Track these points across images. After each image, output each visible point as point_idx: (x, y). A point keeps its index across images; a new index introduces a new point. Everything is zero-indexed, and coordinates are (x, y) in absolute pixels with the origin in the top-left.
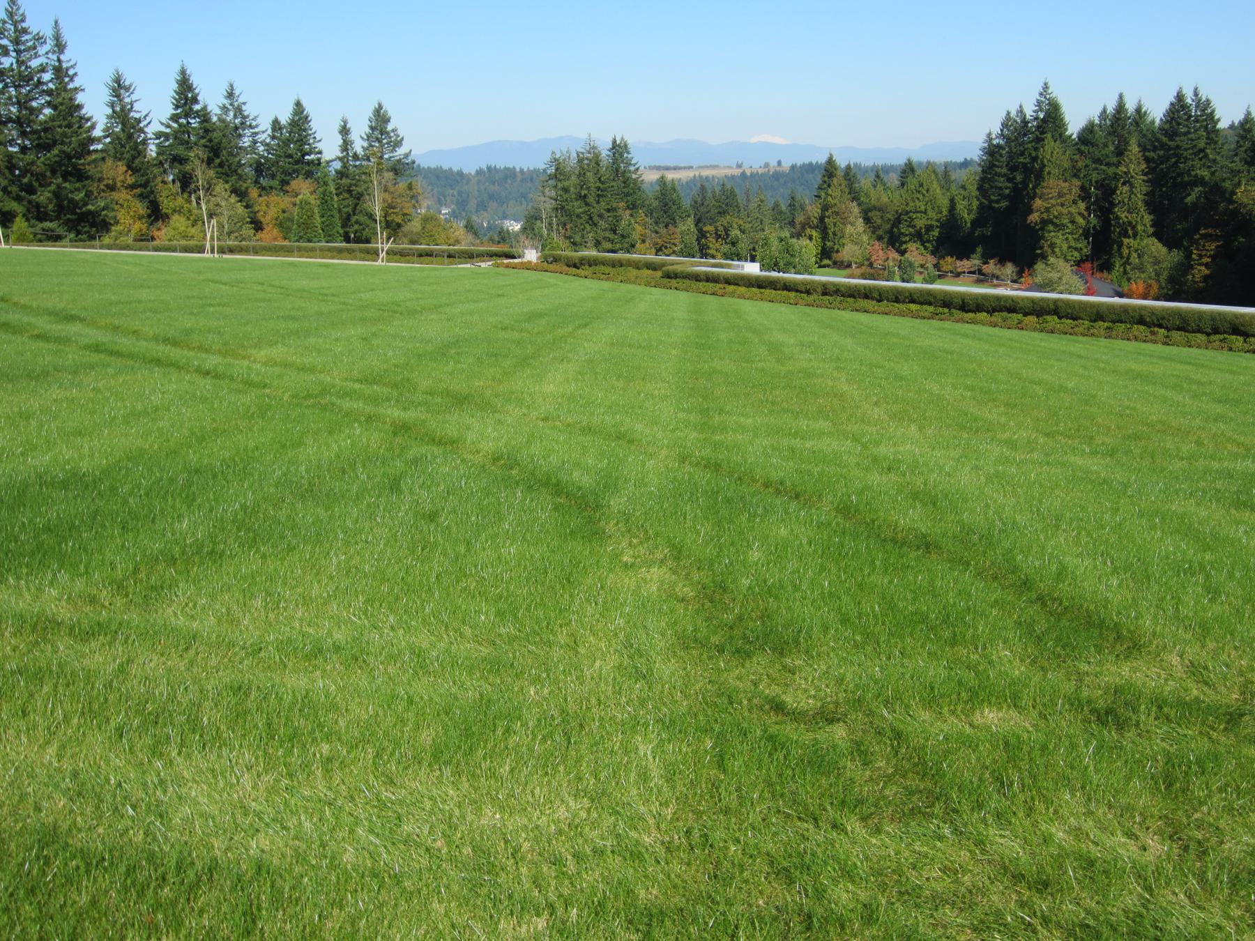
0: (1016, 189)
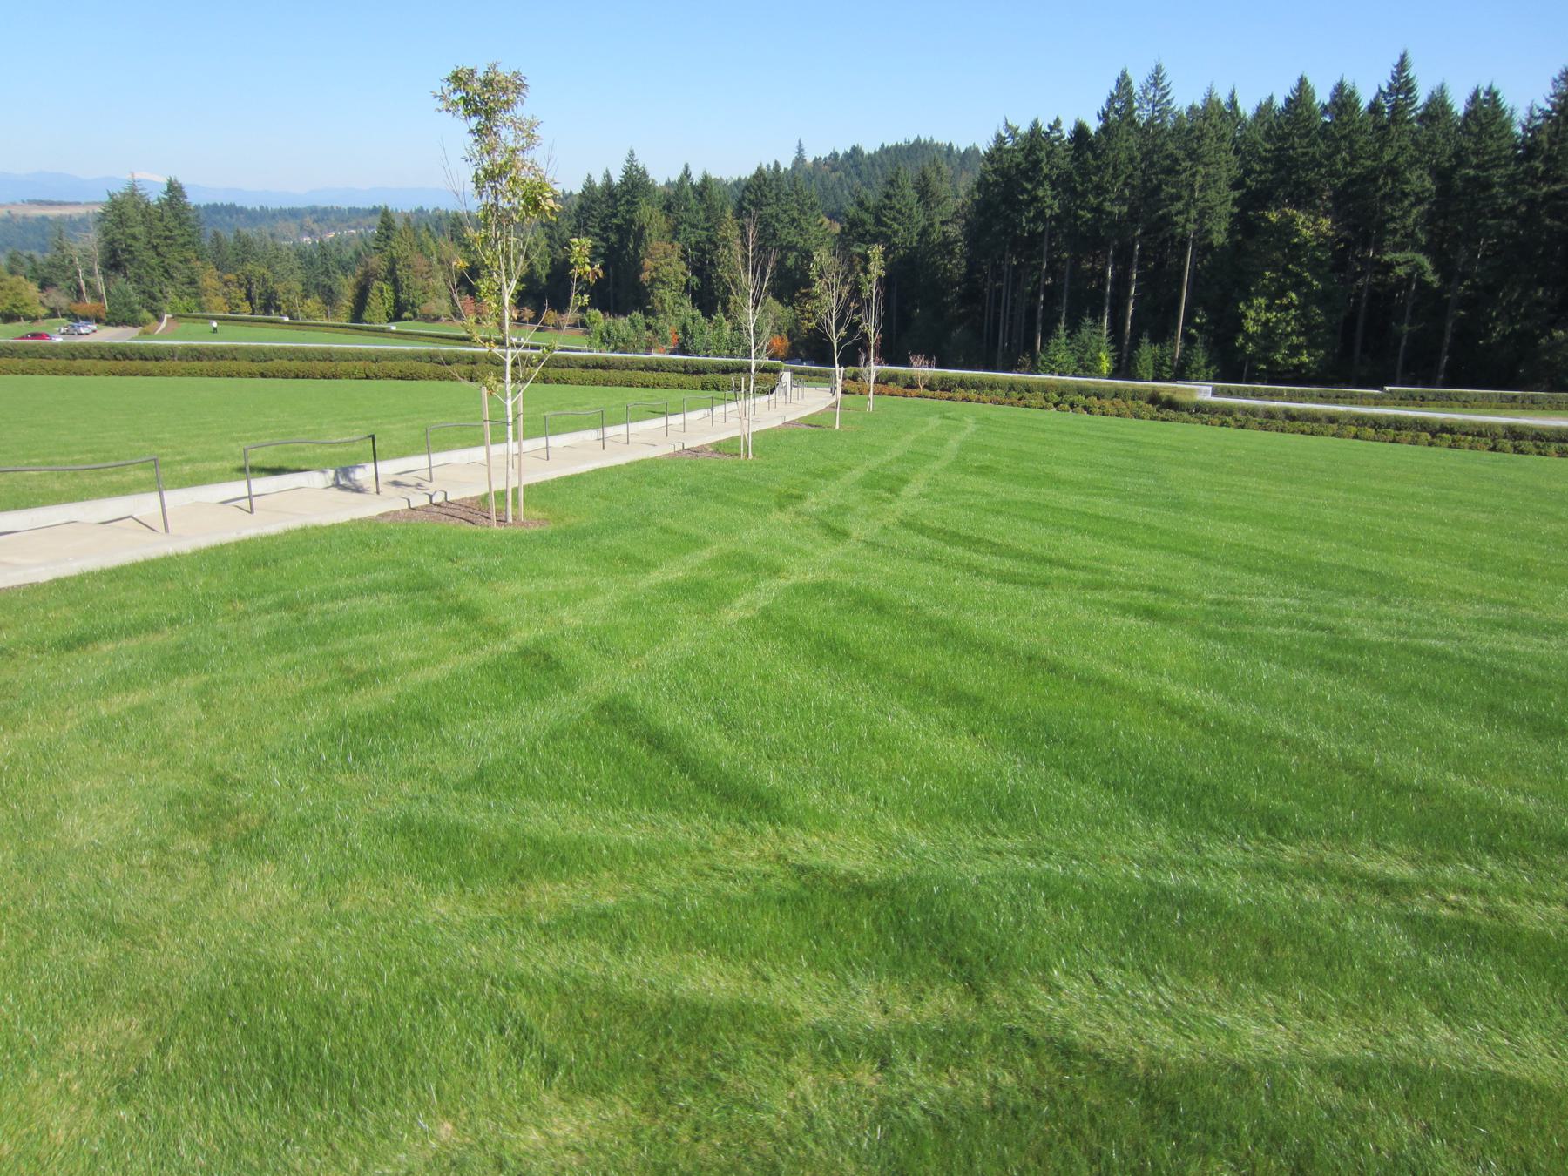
0: (610, 248)
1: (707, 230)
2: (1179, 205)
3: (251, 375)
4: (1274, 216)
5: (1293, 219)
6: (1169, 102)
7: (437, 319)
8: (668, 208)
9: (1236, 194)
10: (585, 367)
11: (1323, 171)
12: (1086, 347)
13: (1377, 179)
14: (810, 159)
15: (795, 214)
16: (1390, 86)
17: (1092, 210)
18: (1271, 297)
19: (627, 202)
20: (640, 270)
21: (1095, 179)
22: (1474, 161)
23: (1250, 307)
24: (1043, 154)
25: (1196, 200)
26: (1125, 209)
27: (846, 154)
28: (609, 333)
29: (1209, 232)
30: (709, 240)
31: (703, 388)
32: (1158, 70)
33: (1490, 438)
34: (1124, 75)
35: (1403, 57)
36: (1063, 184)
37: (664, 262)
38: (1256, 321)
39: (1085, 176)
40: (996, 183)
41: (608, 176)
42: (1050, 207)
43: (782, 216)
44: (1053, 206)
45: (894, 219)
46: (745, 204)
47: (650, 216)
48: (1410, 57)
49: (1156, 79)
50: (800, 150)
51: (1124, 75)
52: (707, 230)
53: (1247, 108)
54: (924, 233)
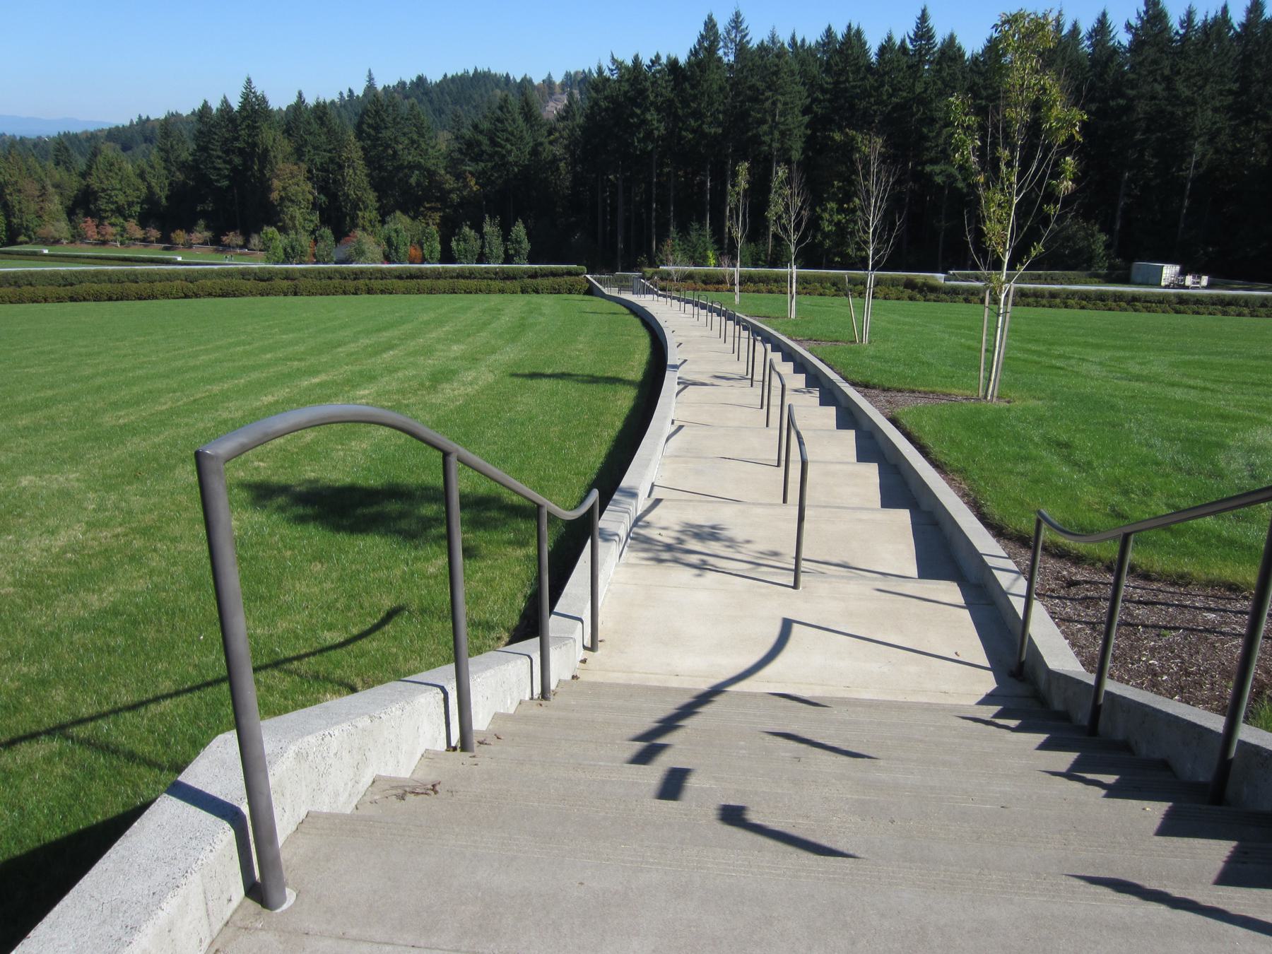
0: (234, 169)
1: (330, 151)
2: (765, 127)
3: (60, 300)
4: (837, 136)
5: (853, 139)
6: (748, 42)
7: (57, 242)
8: (288, 132)
9: (807, 119)
10: (400, 277)
11: (872, 100)
12: (695, 248)
13: (911, 107)
14: (380, 87)
15: (415, 137)
16: (916, 34)
17: (693, 131)
18: (840, 203)
19: (248, 126)
20: (269, 189)
21: (693, 105)
22: (984, 93)
23: (824, 210)
24: (648, 84)
25: (778, 123)
26: (720, 131)
27: (412, 83)
28: (293, 248)
29: (790, 149)
30: (332, 160)
31: (523, 291)
32: (738, 15)
33: (1086, 300)
34: (710, 18)
35: (924, 11)
36: (667, 109)
37: (291, 182)
38: (830, 222)
39: (685, 103)
40: (607, 109)
41: (225, 101)
42: (657, 129)
43: (401, 139)
44: (660, 129)
45: (507, 140)
46: (365, 127)
47: (269, 136)
48: (929, 11)
49: (737, 22)
50: (371, 79)
51: (710, 18)
52: (330, 151)
53: (873, 43)
54: (535, 152)
